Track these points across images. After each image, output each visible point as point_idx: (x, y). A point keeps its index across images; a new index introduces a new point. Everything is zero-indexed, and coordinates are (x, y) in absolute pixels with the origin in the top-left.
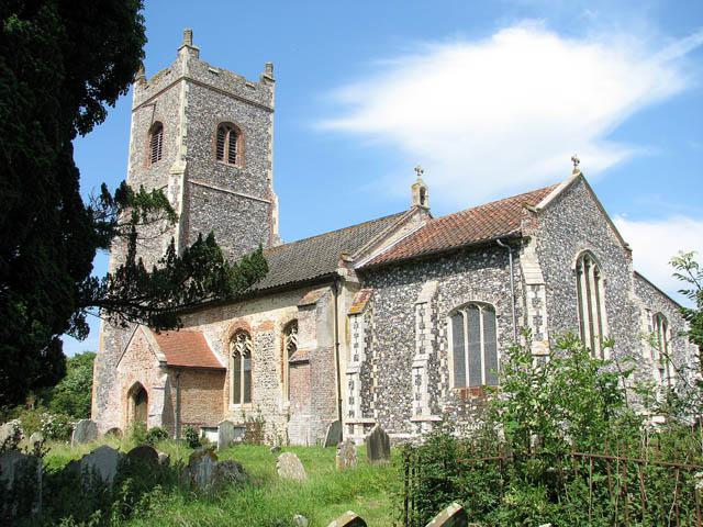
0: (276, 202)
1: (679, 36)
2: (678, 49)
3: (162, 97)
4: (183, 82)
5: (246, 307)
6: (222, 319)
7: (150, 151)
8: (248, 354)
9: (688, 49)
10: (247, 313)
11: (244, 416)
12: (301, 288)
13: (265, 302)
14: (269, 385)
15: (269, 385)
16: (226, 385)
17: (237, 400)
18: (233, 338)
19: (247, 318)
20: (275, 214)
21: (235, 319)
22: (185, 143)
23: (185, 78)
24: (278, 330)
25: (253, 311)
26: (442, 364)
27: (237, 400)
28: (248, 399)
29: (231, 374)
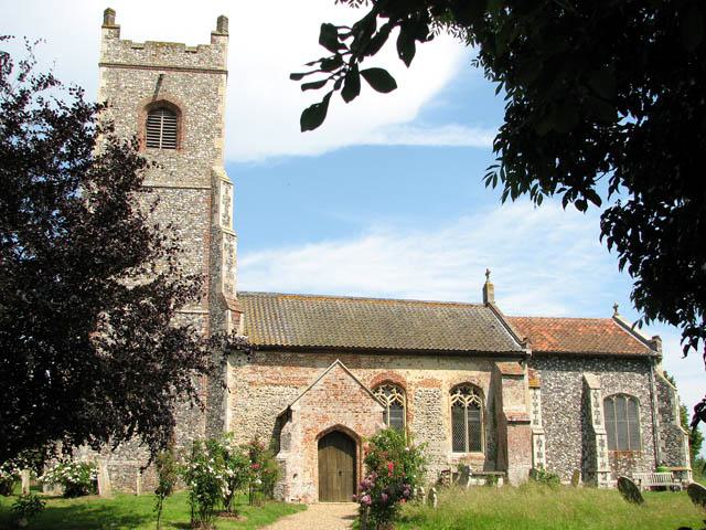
3: (178, 76)
13: (425, 361)
14: (433, 438)
15: (433, 438)
19: (401, 372)
21: (380, 371)
24: (446, 389)
25: (410, 366)
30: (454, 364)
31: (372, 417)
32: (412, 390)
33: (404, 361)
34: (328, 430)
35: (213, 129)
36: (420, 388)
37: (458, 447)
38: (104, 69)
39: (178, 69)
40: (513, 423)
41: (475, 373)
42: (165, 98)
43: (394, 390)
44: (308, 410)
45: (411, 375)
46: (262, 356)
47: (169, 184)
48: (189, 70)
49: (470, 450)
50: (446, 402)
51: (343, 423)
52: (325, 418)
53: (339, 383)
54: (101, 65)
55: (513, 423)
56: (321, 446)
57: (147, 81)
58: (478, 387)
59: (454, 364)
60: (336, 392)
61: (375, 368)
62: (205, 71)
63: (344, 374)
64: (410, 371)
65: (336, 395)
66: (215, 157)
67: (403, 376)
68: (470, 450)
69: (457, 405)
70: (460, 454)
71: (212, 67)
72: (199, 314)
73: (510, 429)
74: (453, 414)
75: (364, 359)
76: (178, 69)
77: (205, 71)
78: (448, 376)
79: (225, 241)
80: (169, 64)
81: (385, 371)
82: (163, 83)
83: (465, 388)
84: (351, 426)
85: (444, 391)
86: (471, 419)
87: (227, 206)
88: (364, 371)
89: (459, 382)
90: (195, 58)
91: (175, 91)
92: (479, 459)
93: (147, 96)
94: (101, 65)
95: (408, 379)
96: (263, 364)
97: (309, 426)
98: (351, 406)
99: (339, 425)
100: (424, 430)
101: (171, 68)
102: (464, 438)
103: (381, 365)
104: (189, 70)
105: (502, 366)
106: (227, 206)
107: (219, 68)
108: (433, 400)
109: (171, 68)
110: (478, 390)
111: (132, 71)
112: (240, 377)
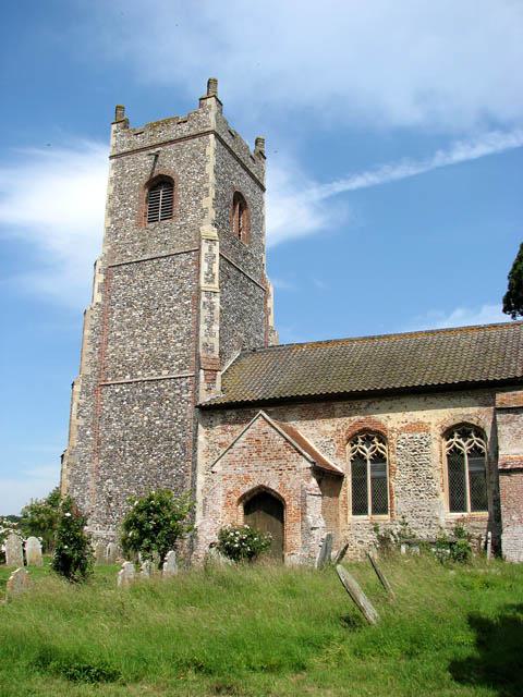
0: (271, 290)
1: (322, 179)
2: (316, 193)
3: (171, 148)
4: (212, 136)
5: (378, 405)
6: (331, 415)
7: (145, 208)
8: (379, 458)
9: (324, 195)
10: (378, 411)
11: (376, 530)
12: (456, 390)
13: (409, 401)
14: (422, 495)
15: (422, 495)
16: (342, 493)
17: (359, 509)
18: (353, 440)
19: (381, 417)
20: (270, 303)
21: (356, 418)
22: (215, 206)
23: (213, 132)
24: (436, 432)
25: (391, 409)
26: (65, 476)
27: (359, 509)
28: (381, 508)
29: (348, 479)
30: (445, 401)
31: (298, 475)
32: (393, 437)
33: (384, 404)
34: (253, 490)
35: (119, 189)
36: (404, 435)
37: (456, 505)
38: (113, 161)
39: (171, 142)
40: (509, 472)
41: (473, 410)
42: (161, 172)
43: (375, 440)
44: (230, 470)
45: (392, 420)
46: (232, 415)
47: (164, 253)
48: (180, 140)
49: (473, 510)
50: (438, 450)
51: (266, 484)
52: (247, 478)
53: (262, 438)
54: (111, 157)
55: (509, 472)
56: (247, 511)
57: (145, 160)
58: (479, 427)
59: (446, 402)
60: (259, 448)
61: (350, 415)
62: (194, 137)
63: (268, 427)
64: (390, 415)
65: (258, 452)
66: (203, 217)
67: (383, 421)
68: (473, 510)
69: (454, 457)
70: (458, 515)
71: (200, 130)
72: (187, 377)
73: (504, 480)
74: (450, 463)
75: (338, 406)
76: (171, 142)
77: (194, 137)
78: (437, 417)
79: (204, 299)
80: (165, 139)
81: (362, 418)
82: (160, 158)
83: (464, 429)
84: (274, 486)
85: (433, 435)
86: (475, 469)
87: (211, 264)
88: (339, 420)
89: (452, 423)
90: (185, 127)
91: (169, 165)
92: (482, 520)
93: (145, 176)
94: (111, 157)
95: (389, 426)
96: (234, 423)
97: (230, 488)
98: (274, 463)
99: (261, 487)
100: (410, 486)
101: (166, 143)
102: (464, 494)
103: (358, 411)
104: (180, 140)
105: (502, 398)
106: (211, 264)
107: (207, 130)
108: (420, 449)
109: (166, 143)
110: (480, 432)
111: (134, 156)
112: (212, 438)
